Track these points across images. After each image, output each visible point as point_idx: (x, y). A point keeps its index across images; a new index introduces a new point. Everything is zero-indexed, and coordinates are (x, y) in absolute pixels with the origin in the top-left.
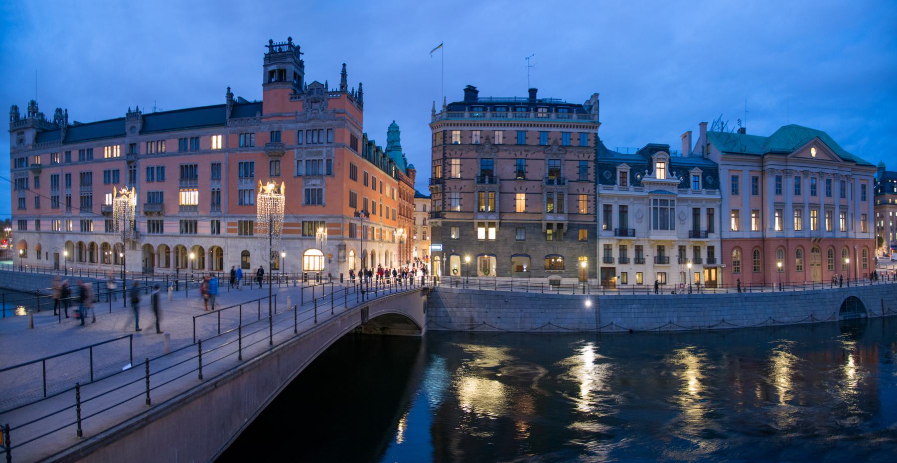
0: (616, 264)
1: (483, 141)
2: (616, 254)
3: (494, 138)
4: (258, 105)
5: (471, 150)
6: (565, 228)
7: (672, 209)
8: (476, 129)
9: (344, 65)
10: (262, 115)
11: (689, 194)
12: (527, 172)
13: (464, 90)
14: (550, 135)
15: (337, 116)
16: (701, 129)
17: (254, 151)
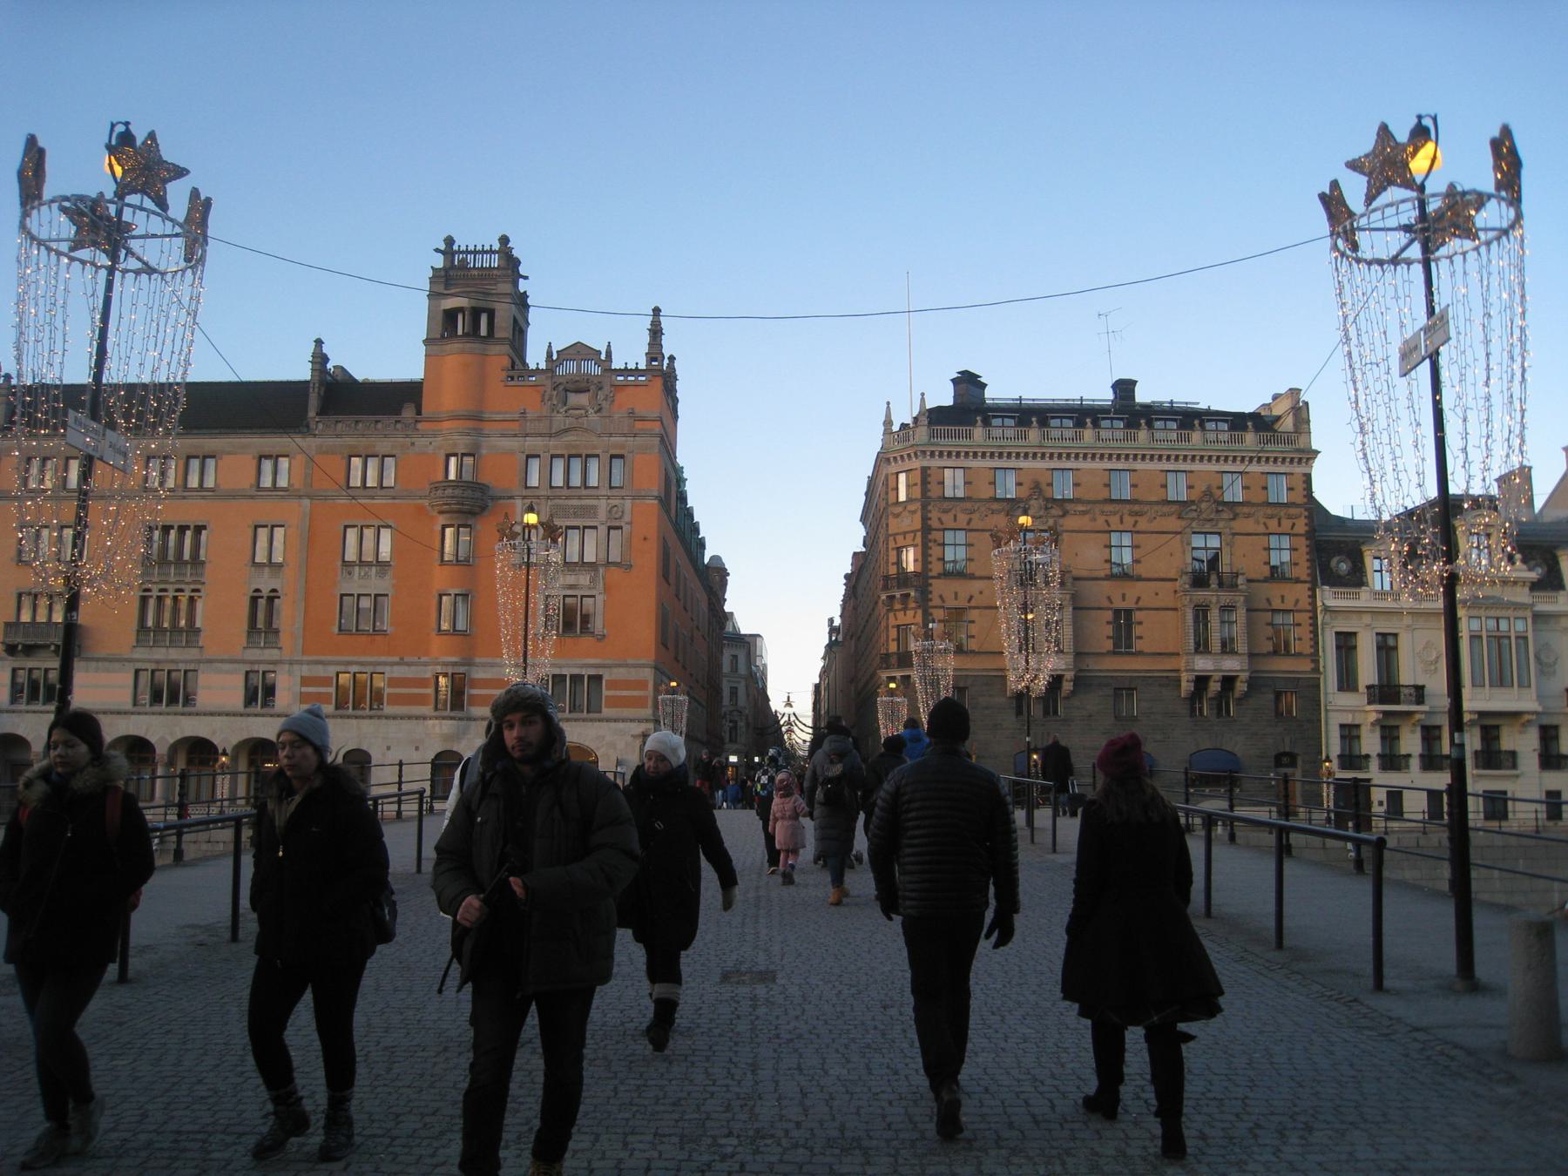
0: (1374, 773)
2: (1370, 744)
6: (1241, 687)
8: (1005, 465)
10: (419, 412)
13: (953, 380)
15: (639, 425)
17: (394, 498)
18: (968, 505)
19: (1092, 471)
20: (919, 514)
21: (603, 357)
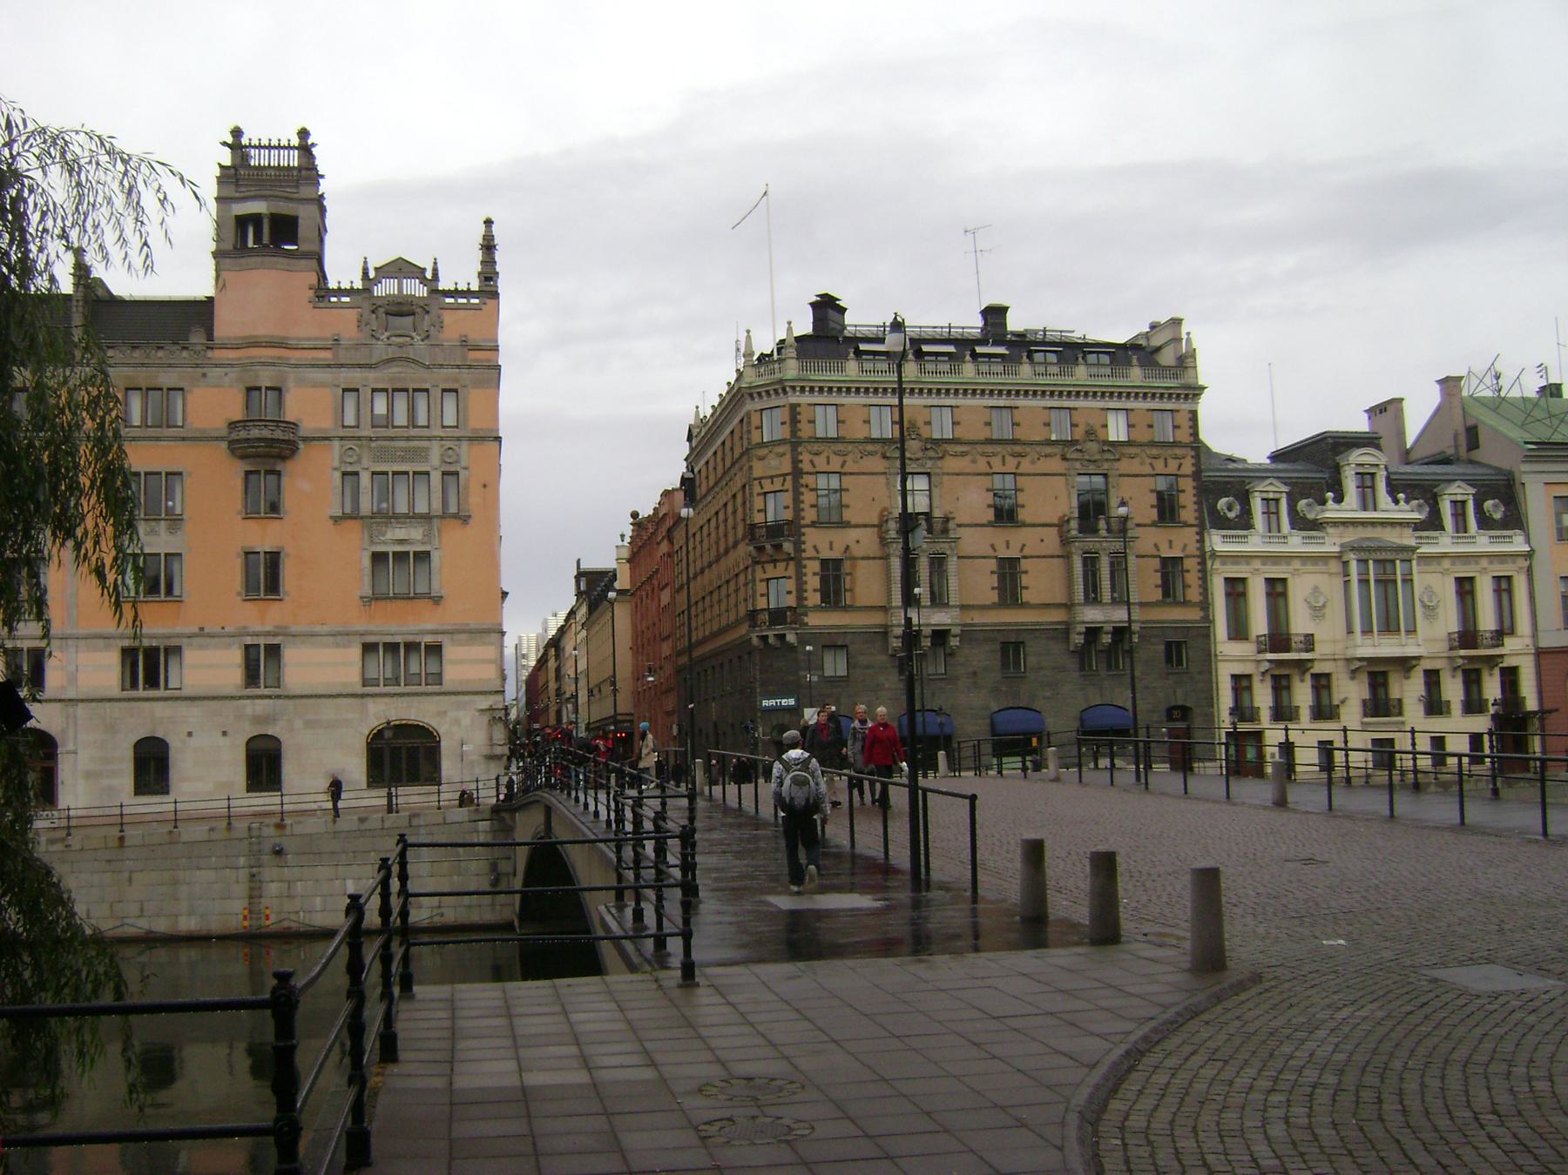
1: (1079, 434)
3: (928, 423)
4: (197, 313)
5: (871, 454)
7: (1408, 581)
9: (489, 223)
10: (210, 337)
11: (1445, 543)
12: (1023, 506)
13: (812, 305)
14: (1077, 417)
16: (1441, 390)
18: (840, 447)
21: (429, 275)
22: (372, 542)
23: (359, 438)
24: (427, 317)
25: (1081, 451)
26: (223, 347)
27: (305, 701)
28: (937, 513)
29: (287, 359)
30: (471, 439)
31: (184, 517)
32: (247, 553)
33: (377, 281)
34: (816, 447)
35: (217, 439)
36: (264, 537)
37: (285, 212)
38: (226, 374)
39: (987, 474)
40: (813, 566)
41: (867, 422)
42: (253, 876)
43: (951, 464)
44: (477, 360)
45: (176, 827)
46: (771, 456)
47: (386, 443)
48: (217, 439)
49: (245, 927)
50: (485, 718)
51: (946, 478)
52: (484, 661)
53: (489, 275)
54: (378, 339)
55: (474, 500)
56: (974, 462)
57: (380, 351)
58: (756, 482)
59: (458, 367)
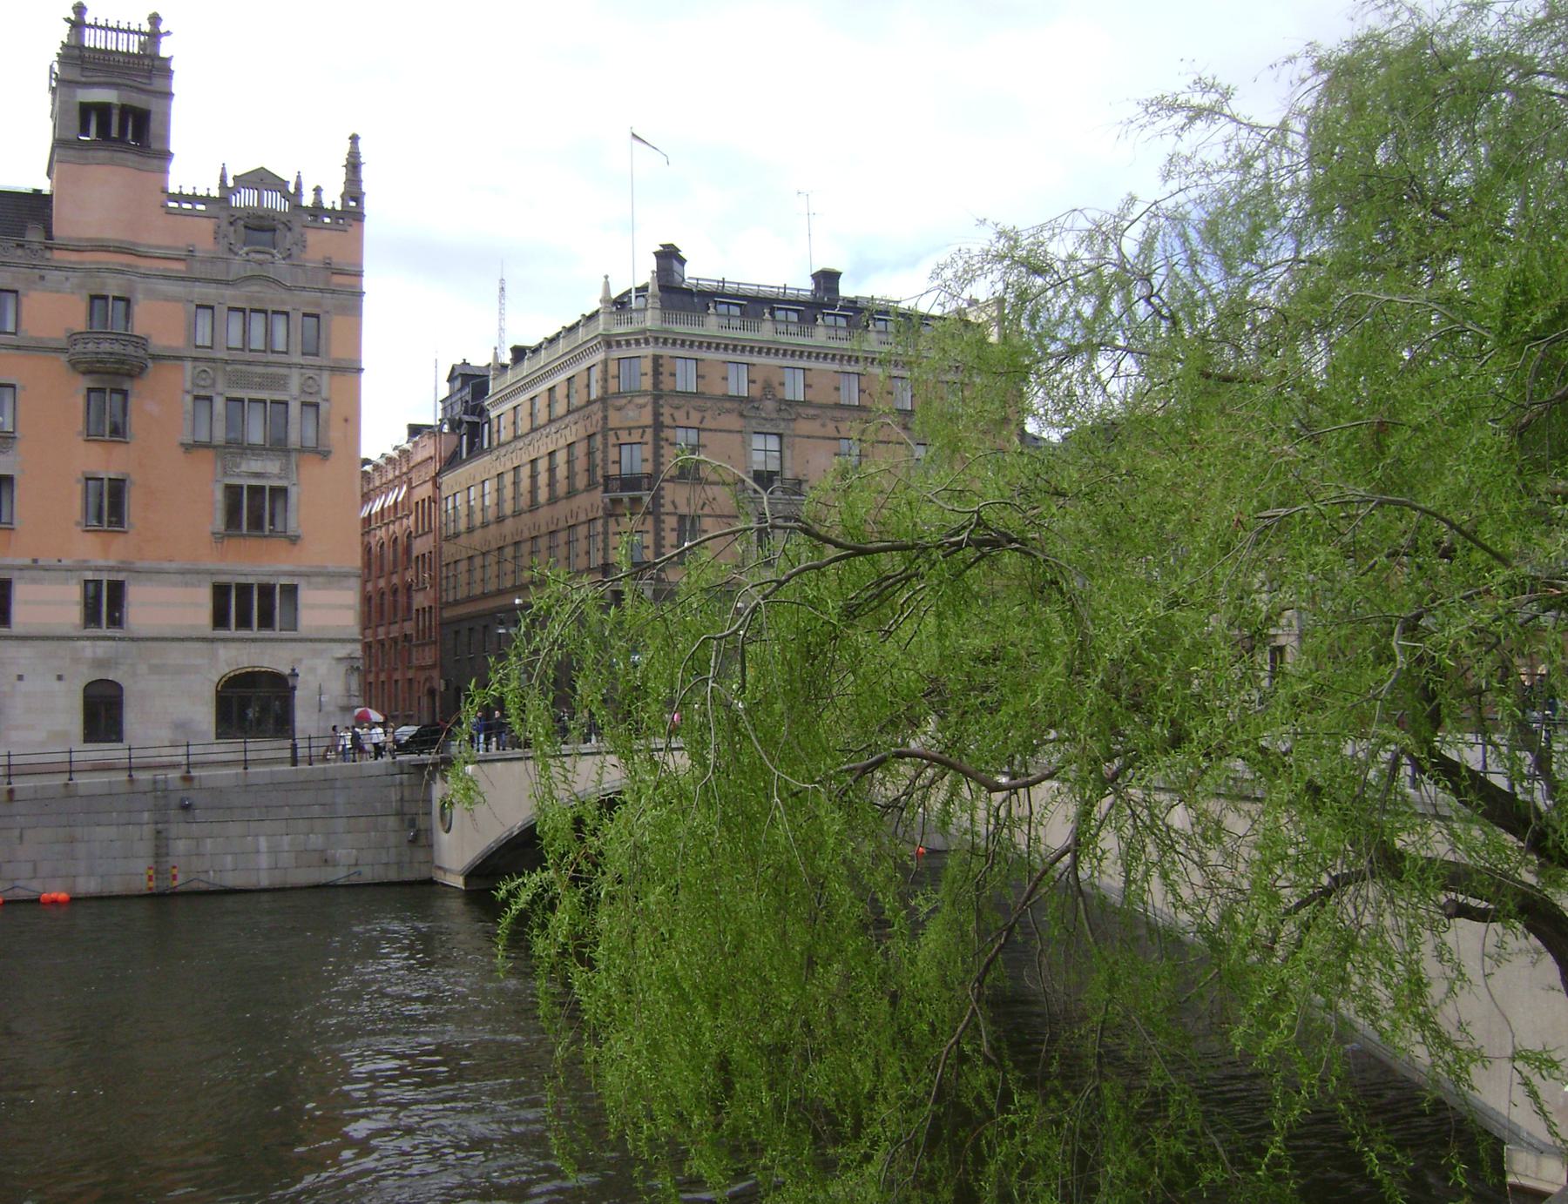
1: (756, 391)
4: (34, 206)
5: (728, 411)
9: (354, 139)
13: (656, 254)
15: (337, 279)
18: (699, 402)
19: (823, 372)
20: (649, 409)
21: (292, 189)
22: (225, 473)
23: (214, 360)
24: (288, 234)
25: (758, 408)
26: (64, 248)
27: (149, 644)
28: (788, 474)
29: (137, 267)
30: (333, 369)
31: (17, 434)
32: (88, 479)
33: (235, 191)
34: (676, 402)
35: (56, 350)
36: (105, 461)
37: (136, 104)
38: (67, 279)
39: (835, 439)
40: (671, 522)
41: (725, 379)
42: (159, 832)
43: (804, 427)
44: (340, 285)
45: (71, 779)
46: (630, 406)
47: (243, 367)
48: (56, 350)
49: (150, 889)
50: (342, 668)
51: (797, 439)
52: (341, 607)
53: (354, 191)
54: (236, 254)
55: (335, 435)
56: (823, 425)
57: (238, 267)
58: (612, 433)
59: (321, 291)
